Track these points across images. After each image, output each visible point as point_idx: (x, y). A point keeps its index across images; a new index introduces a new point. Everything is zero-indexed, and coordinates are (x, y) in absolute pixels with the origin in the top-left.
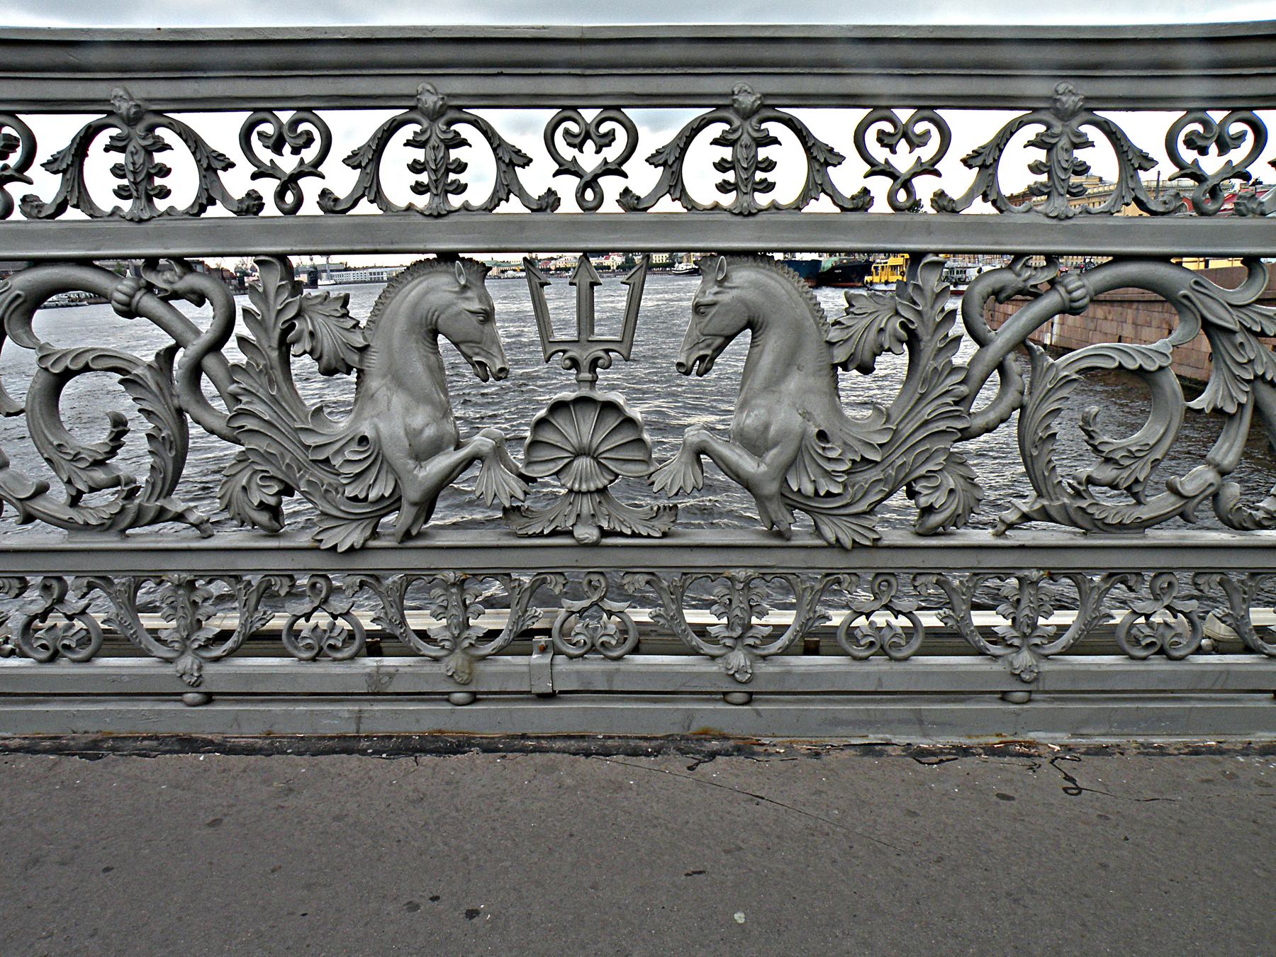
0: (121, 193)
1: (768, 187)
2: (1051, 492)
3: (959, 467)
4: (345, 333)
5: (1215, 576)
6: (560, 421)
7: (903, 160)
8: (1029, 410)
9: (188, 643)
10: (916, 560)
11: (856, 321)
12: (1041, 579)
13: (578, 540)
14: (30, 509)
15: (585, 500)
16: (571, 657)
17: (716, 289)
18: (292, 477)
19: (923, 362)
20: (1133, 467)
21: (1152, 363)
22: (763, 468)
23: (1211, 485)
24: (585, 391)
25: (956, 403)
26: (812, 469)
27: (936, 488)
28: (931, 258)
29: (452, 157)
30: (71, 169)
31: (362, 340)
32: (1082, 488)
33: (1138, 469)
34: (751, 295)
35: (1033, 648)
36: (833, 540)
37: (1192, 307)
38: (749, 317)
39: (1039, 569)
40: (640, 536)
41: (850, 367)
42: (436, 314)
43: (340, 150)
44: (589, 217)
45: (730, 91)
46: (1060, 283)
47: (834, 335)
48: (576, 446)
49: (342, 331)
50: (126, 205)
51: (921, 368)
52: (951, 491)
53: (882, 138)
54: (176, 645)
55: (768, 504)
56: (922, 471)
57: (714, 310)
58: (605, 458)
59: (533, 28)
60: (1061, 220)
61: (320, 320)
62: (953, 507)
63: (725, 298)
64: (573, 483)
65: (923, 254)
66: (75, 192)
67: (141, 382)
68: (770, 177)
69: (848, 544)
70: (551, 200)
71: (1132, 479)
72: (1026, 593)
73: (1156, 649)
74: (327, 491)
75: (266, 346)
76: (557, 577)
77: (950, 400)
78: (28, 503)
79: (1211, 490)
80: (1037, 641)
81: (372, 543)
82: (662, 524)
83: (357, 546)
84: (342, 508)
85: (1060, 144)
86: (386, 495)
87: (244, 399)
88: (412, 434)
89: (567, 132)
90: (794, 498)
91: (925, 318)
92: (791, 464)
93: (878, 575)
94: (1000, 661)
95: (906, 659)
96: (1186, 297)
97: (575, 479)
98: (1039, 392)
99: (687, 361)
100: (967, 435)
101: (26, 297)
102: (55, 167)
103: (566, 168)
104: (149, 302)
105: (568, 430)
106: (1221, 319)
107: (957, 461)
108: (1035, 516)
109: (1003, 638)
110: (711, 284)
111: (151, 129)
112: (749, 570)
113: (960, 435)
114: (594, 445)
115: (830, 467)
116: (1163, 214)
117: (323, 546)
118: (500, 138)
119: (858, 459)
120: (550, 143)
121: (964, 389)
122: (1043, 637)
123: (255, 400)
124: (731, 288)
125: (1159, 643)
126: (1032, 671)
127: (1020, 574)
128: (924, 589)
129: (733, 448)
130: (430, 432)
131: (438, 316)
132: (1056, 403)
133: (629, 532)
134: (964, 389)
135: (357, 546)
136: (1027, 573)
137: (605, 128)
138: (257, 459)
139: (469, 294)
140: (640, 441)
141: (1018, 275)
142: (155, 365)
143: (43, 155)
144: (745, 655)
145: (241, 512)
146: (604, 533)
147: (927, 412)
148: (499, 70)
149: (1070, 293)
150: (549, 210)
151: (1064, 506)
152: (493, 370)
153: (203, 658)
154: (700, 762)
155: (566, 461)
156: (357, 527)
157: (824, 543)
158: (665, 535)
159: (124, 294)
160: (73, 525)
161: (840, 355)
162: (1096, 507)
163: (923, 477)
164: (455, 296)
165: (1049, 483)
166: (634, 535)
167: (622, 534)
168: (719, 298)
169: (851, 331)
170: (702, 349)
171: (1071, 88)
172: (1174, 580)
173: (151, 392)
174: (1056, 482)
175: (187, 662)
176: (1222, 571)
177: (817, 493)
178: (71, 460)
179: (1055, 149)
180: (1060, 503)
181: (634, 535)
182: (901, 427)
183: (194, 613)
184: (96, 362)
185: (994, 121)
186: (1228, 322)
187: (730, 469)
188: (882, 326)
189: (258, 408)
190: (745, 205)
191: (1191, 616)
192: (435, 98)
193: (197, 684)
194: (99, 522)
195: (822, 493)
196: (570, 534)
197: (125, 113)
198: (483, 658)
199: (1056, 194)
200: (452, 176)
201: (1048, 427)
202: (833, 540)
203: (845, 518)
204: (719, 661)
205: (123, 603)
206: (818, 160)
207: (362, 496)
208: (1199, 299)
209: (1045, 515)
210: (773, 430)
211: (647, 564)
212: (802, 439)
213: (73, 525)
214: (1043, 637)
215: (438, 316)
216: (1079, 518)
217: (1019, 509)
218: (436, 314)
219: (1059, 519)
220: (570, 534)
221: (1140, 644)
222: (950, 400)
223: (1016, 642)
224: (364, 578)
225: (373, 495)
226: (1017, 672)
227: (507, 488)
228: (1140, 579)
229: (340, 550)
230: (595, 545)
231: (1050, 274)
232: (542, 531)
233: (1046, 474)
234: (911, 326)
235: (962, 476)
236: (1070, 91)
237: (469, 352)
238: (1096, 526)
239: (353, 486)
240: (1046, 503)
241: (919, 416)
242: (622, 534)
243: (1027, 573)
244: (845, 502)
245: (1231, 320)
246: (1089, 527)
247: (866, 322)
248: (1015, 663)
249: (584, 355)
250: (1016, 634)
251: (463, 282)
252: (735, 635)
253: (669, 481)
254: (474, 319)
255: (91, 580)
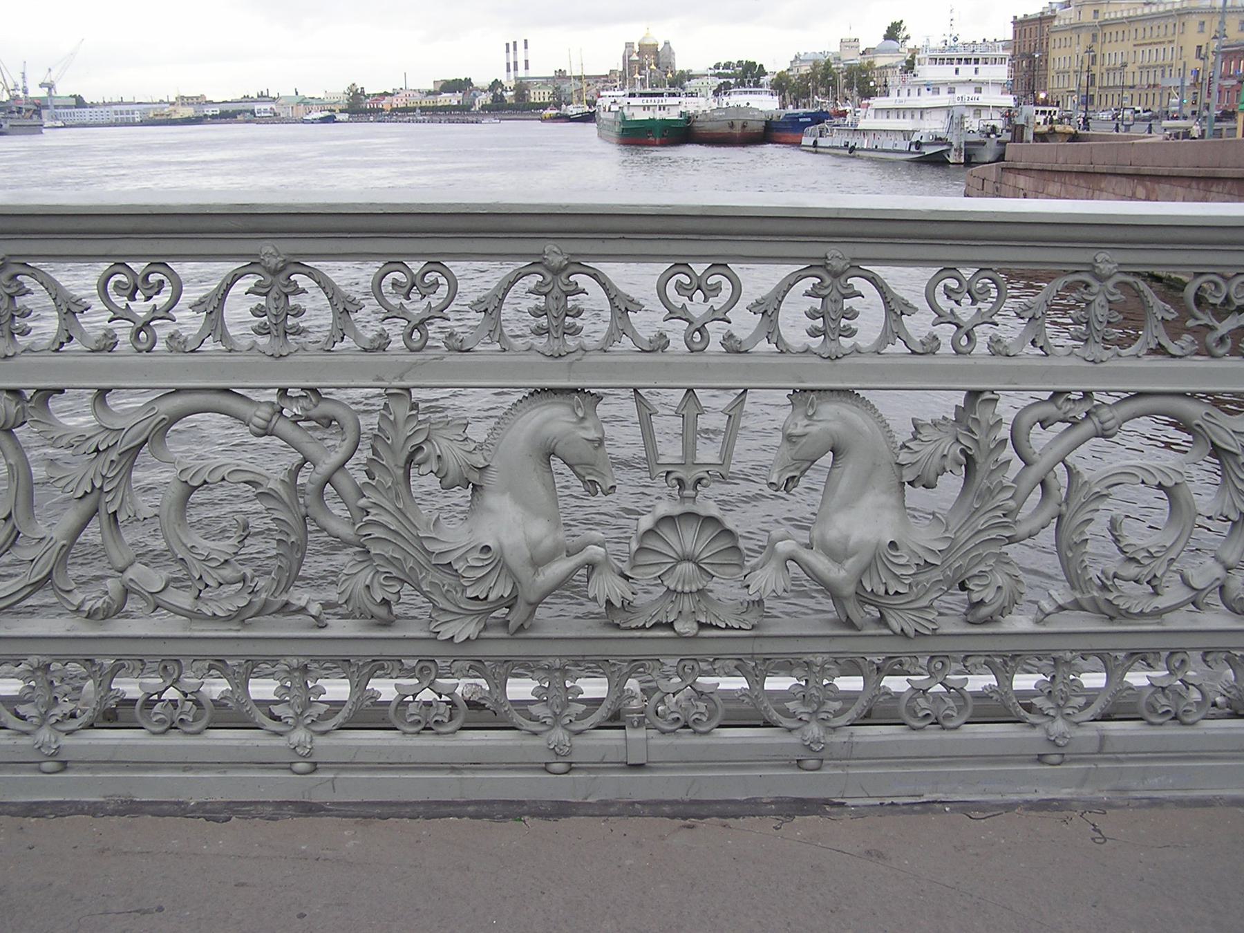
0: (261, 330)
1: (851, 333)
2: (1083, 586)
3: (1006, 566)
4: (469, 455)
5: (1221, 654)
6: (667, 532)
7: (966, 312)
8: (1065, 519)
9: (300, 718)
10: (971, 645)
11: (923, 447)
12: (1074, 658)
13: (678, 634)
14: (159, 601)
15: (686, 598)
16: (663, 732)
17: (806, 422)
18: (414, 578)
19: (978, 479)
20: (1152, 565)
21: (1170, 481)
22: (843, 573)
23: (1218, 579)
24: (688, 507)
25: (1005, 515)
26: (883, 572)
27: (986, 586)
28: (988, 396)
29: (569, 305)
30: (216, 310)
31: (483, 461)
32: (1109, 583)
33: (1157, 567)
34: (835, 426)
35: (1065, 717)
36: (898, 630)
37: (1203, 433)
38: (834, 444)
39: (1072, 651)
40: (733, 628)
41: (916, 485)
42: (555, 441)
43: (191, 295)
44: (694, 358)
45: (823, 256)
46: (1094, 413)
47: (904, 457)
48: (680, 553)
49: (465, 453)
50: (263, 341)
51: (976, 485)
52: (999, 588)
53: (949, 292)
54: (290, 721)
55: (845, 602)
56: (975, 571)
57: (804, 440)
58: (705, 563)
59: (658, 206)
60: (1096, 363)
61: (445, 443)
62: (1000, 601)
63: (814, 429)
64: (677, 584)
65: (981, 392)
66: (494, 328)
67: (275, 495)
68: (853, 324)
69: (912, 633)
70: (660, 344)
71: (1152, 575)
72: (1061, 669)
73: (1170, 717)
74: (448, 591)
75: (393, 465)
76: (655, 663)
77: (1000, 513)
78: (158, 596)
79: (1218, 583)
80: (1070, 711)
81: (485, 634)
82: (752, 618)
83: (473, 637)
84: (462, 606)
85: (1097, 302)
86: (506, 596)
87: (372, 511)
88: (533, 545)
89: (395, 284)
90: (869, 597)
91: (981, 444)
92: (867, 569)
93: (932, 657)
94: (1037, 729)
95: (956, 728)
96: (1198, 425)
97: (678, 581)
98: (1074, 504)
99: (779, 481)
100: (1013, 541)
101: (170, 419)
102: (477, 308)
103: (673, 314)
104: (283, 426)
105: (672, 540)
106: (1226, 444)
107: (1002, 559)
108: (1068, 606)
109: (1040, 709)
110: (800, 417)
111: (14, 277)
112: (824, 655)
113: (1007, 541)
114: (697, 553)
115: (898, 571)
116: (1181, 357)
117: (440, 637)
118: (616, 289)
119: (922, 563)
120: (663, 295)
121: (1012, 503)
122: (1075, 708)
123: (382, 512)
124: (820, 421)
125: (1173, 711)
126: (1065, 737)
127: (1054, 655)
128: (974, 668)
129: (817, 555)
130: (548, 543)
131: (556, 444)
132: (1090, 514)
133: (724, 626)
134: (1012, 503)
135: (473, 637)
136: (1061, 654)
137: (712, 280)
138: (381, 562)
139: (587, 424)
140: (736, 548)
141: (1060, 409)
142: (287, 480)
143: (746, 299)
144: (819, 727)
145: (362, 607)
146: (702, 626)
147: (981, 523)
148: (622, 236)
149: (1102, 423)
150: (660, 350)
151: (1093, 598)
152: (604, 488)
153: (314, 731)
154: (783, 822)
155: (671, 565)
156: (472, 621)
157: (890, 633)
158: (753, 627)
159: (264, 420)
160: (201, 616)
161: (908, 475)
162: (1121, 599)
163: (975, 576)
164: (572, 425)
165: (1081, 579)
166: (728, 627)
167: (717, 627)
168: (808, 429)
169: (922, 453)
170: (791, 471)
171: (1108, 257)
172: (1186, 657)
173: (283, 502)
174: (1087, 578)
175: (300, 735)
176: (1228, 650)
177: (887, 592)
178: (204, 560)
179: (1093, 304)
180: (1090, 596)
181: (728, 627)
182: (958, 534)
183: (51, 691)
184: (231, 476)
185: (496, 273)
186: (1231, 446)
187: (813, 573)
188: (945, 453)
189: (384, 518)
190: (833, 350)
191: (1200, 687)
192: (561, 258)
193: (310, 754)
194: (228, 614)
195: (891, 592)
196: (670, 626)
197: (273, 267)
198: (579, 733)
199: (1093, 341)
200: (844, 322)
201: (1083, 533)
202: (898, 630)
203: (909, 612)
204: (796, 733)
205: (240, 683)
206: (896, 313)
207: (482, 597)
208: (1208, 427)
209: (1078, 605)
210: (851, 543)
211: (737, 651)
212: (877, 548)
213: (201, 616)
214: (1075, 708)
215: (556, 444)
216: (1104, 607)
217: (1056, 602)
218: (555, 441)
219: (1087, 607)
220: (670, 626)
221: (1157, 712)
222: (1000, 513)
223: (1052, 712)
224: (472, 663)
225: (492, 597)
226: (1053, 738)
227: (618, 591)
228: (1157, 656)
229: (456, 640)
230: (695, 637)
231: (1087, 406)
232: (644, 625)
233: (1079, 572)
234: (969, 452)
235: (1008, 575)
236: (1107, 261)
237: (583, 473)
238: (1121, 614)
239: (475, 587)
240: (1079, 596)
241: (974, 525)
242: (717, 627)
243: (1061, 654)
244: (910, 599)
245: (1235, 445)
246: (1113, 614)
247: (931, 447)
248: (1051, 730)
249: (689, 476)
250: (1051, 705)
251: (581, 414)
252: (810, 710)
253: (763, 584)
254: (590, 446)
255: (212, 663)
